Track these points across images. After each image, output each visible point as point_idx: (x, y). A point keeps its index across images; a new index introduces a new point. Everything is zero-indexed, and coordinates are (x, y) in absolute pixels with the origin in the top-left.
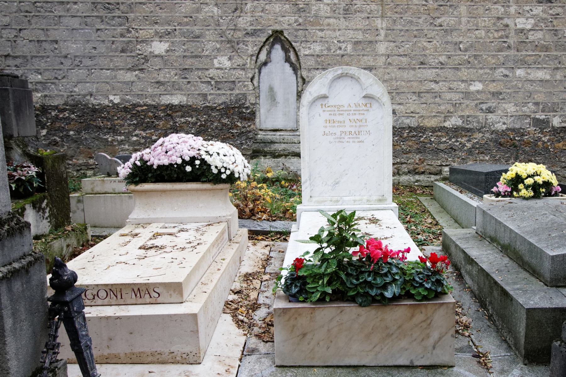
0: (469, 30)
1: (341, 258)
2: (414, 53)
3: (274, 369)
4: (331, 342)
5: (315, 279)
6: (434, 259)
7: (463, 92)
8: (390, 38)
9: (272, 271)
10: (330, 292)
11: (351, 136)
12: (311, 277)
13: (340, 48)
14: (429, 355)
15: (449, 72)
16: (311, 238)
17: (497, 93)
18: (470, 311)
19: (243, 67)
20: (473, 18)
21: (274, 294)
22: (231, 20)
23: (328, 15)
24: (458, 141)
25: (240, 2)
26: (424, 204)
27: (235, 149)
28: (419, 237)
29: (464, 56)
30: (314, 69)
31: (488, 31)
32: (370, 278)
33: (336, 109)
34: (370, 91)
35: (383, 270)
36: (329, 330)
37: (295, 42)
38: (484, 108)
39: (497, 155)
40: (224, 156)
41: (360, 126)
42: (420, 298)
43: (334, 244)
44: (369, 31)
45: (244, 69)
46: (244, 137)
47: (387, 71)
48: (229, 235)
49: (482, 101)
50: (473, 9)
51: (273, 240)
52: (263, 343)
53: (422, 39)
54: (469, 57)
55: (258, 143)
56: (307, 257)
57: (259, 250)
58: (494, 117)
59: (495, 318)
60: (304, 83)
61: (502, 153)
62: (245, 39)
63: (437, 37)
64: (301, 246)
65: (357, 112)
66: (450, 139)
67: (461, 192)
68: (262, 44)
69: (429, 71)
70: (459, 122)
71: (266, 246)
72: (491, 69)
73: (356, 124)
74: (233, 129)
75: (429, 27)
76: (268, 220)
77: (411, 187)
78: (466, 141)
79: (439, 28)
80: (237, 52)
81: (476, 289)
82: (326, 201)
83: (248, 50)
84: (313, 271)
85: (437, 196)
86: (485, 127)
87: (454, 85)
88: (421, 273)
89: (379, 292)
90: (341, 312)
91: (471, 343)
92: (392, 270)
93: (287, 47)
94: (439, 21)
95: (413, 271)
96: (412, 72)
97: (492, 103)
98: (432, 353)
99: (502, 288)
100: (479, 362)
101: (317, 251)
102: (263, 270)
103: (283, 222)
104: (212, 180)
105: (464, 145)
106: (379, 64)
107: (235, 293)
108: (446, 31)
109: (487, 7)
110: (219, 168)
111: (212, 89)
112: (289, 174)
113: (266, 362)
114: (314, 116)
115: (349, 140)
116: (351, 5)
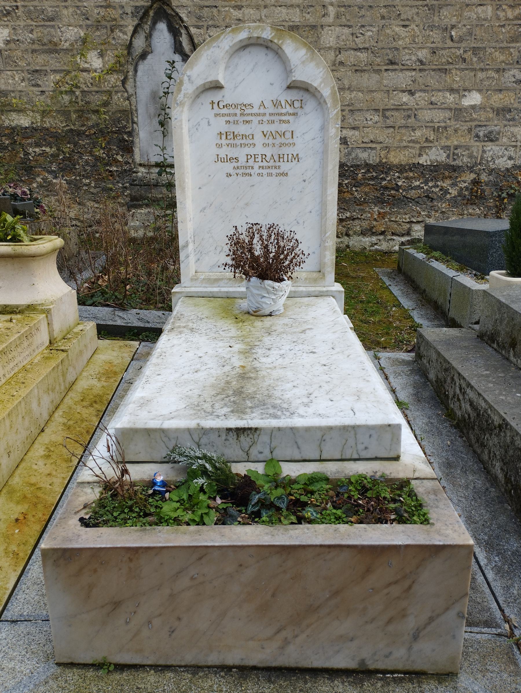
2: (380, 45)
4: (179, 619)
7: (451, 109)
11: (265, 164)
17: (503, 110)
24: (438, 186)
33: (238, 112)
38: (481, 134)
41: (281, 145)
49: (480, 123)
53: (393, 22)
54: (465, 52)
58: (496, 148)
65: (276, 118)
66: (426, 183)
72: (498, 71)
73: (274, 141)
74: (111, 165)
86: (480, 164)
90: (200, 558)
96: (375, 77)
105: (447, 192)
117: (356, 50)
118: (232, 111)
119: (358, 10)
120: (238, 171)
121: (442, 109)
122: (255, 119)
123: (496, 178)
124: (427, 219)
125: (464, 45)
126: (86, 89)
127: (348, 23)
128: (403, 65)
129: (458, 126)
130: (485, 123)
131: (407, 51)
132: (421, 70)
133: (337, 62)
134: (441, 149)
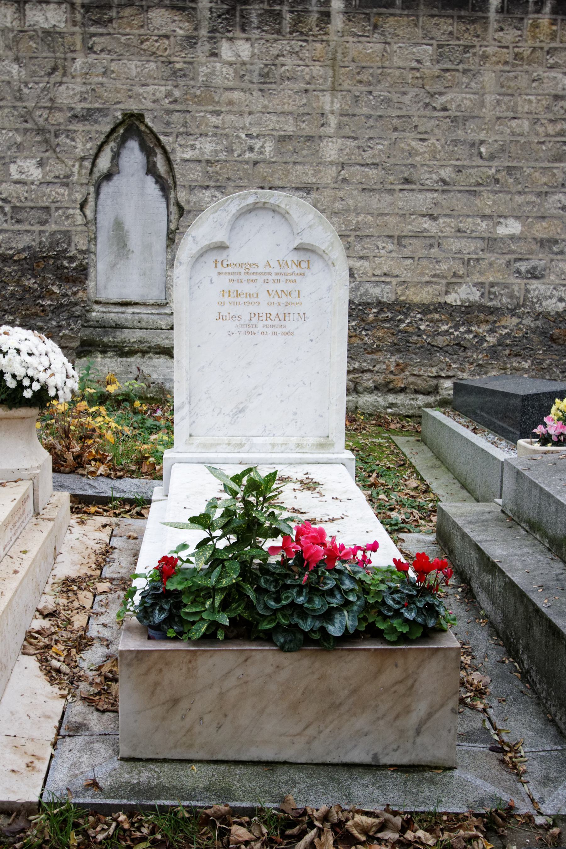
0: (499, 118)
1: (247, 558)
2: (392, 161)
3: (117, 764)
5: (199, 596)
6: (422, 564)
7: (483, 239)
8: (347, 131)
9: (115, 576)
10: (226, 622)
11: (269, 322)
12: (191, 593)
13: (251, 149)
14: (409, 745)
15: (458, 200)
16: (193, 520)
17: (549, 241)
18: (486, 663)
19: (65, 181)
20: (508, 95)
21: (120, 623)
22: (43, 90)
23: (230, 84)
24: (471, 332)
25: (63, 56)
26: (404, 450)
27: (49, 342)
28: (394, 514)
29: (487, 169)
30: (201, 187)
31: (536, 121)
32: (302, 598)
33: (242, 271)
34: (307, 239)
35: (325, 584)
36: (221, 694)
37: (166, 134)
38: (523, 269)
39: (544, 360)
40: (30, 355)
41: (287, 304)
42: (393, 638)
43: (234, 532)
44: (308, 117)
45: (66, 185)
46: (64, 315)
47: (341, 194)
48: (35, 505)
49: (520, 256)
50: (508, 79)
51: (116, 515)
52: (95, 713)
53: (408, 134)
54: (498, 171)
55: (90, 327)
56: (184, 555)
57: (90, 533)
58: (542, 287)
59: (535, 677)
60: (181, 215)
61: (554, 357)
62: (71, 127)
63: (436, 131)
64: (171, 528)
65: (283, 278)
66: (456, 327)
67: (475, 431)
68: (103, 137)
69: (420, 196)
70: (475, 296)
71: (105, 526)
72: (539, 194)
73: (280, 300)
74: (43, 298)
75: (422, 112)
76: (108, 476)
77: (379, 417)
78: (487, 332)
79: (442, 114)
80: (55, 151)
81: (499, 619)
82: (218, 444)
83: (75, 147)
84: (194, 582)
85: (429, 436)
86: (523, 306)
87: (467, 224)
88: (396, 591)
89: (318, 624)
90: (246, 660)
91: (488, 725)
92: (343, 584)
93: (151, 145)
94: (443, 99)
95: (383, 587)
96: (388, 198)
97: (539, 260)
98: (414, 743)
99: (550, 621)
100: (503, 761)
101: (202, 544)
102: (98, 572)
103: (136, 481)
104: (5, 400)
105: (483, 340)
106: (324, 181)
107: (45, 617)
108: (454, 120)
109: (535, 74)
110: (18, 379)
111: (6, 221)
112: (149, 386)
113: (103, 750)
114: (200, 282)
115: (265, 330)
116: (275, 65)
117: (363, 165)
118: (236, 270)
119: (364, 120)
120: (241, 329)
121: (472, 237)
122: (260, 279)
123: (544, 323)
124: (459, 373)
125: (496, 164)
126: (18, 204)
127: (353, 135)
128: (422, 185)
129: (493, 259)
130: (528, 256)
131: (425, 168)
132: (444, 191)
133: (340, 179)
134: (474, 286)
